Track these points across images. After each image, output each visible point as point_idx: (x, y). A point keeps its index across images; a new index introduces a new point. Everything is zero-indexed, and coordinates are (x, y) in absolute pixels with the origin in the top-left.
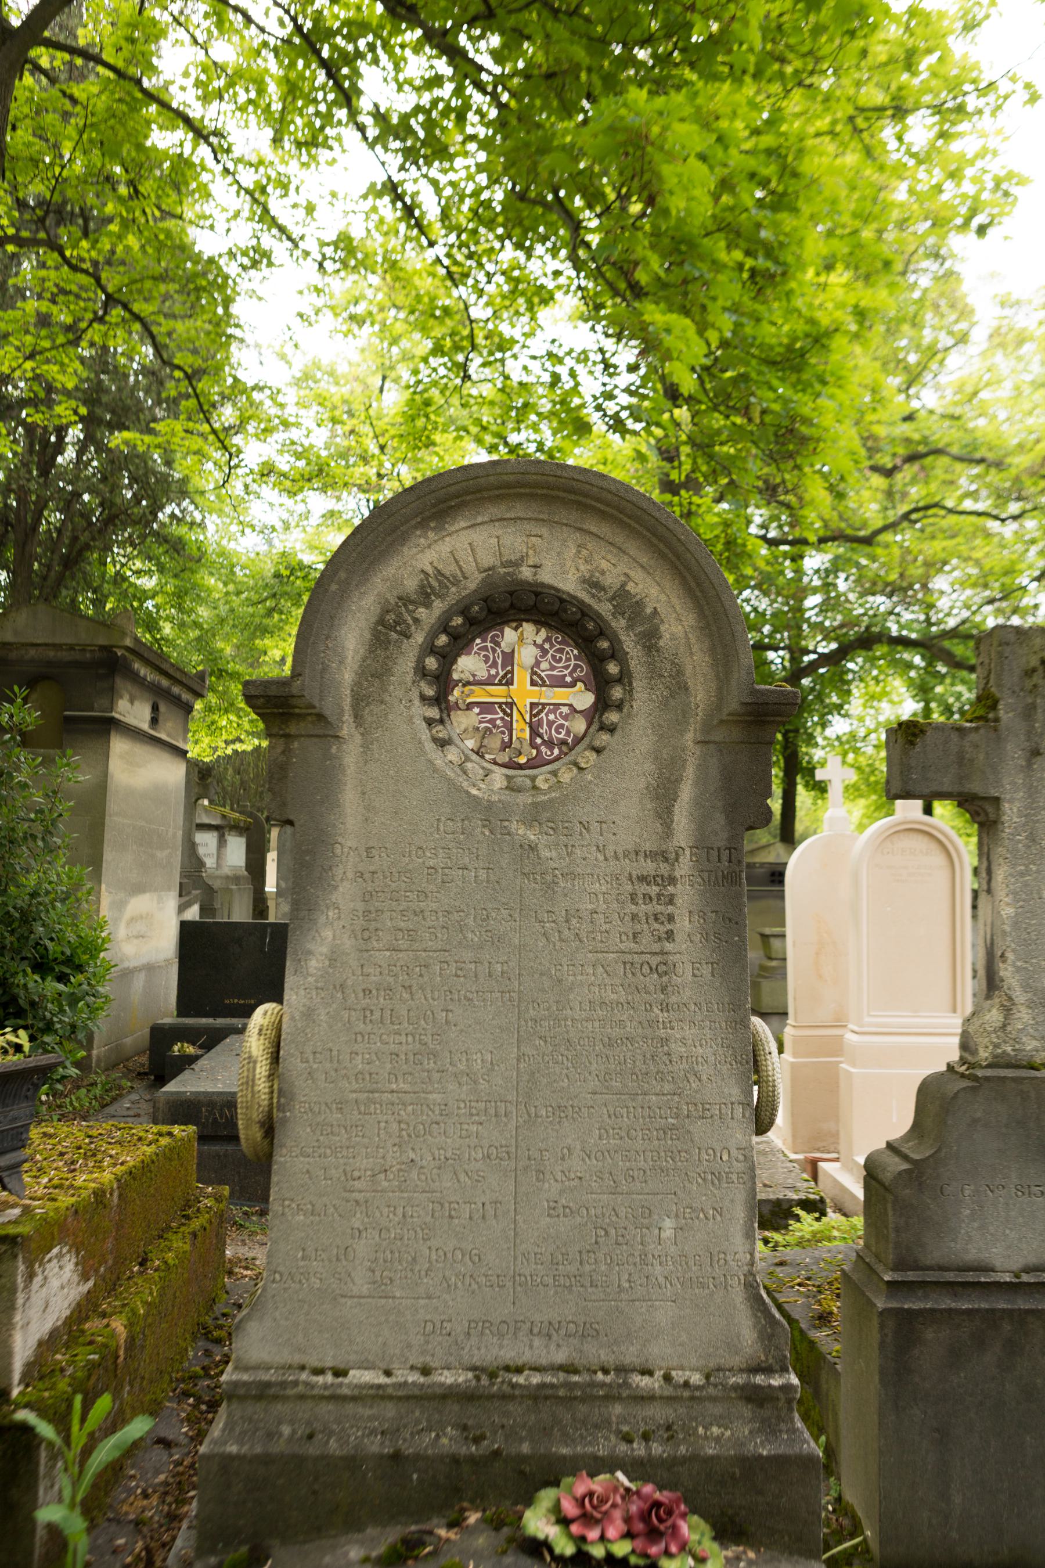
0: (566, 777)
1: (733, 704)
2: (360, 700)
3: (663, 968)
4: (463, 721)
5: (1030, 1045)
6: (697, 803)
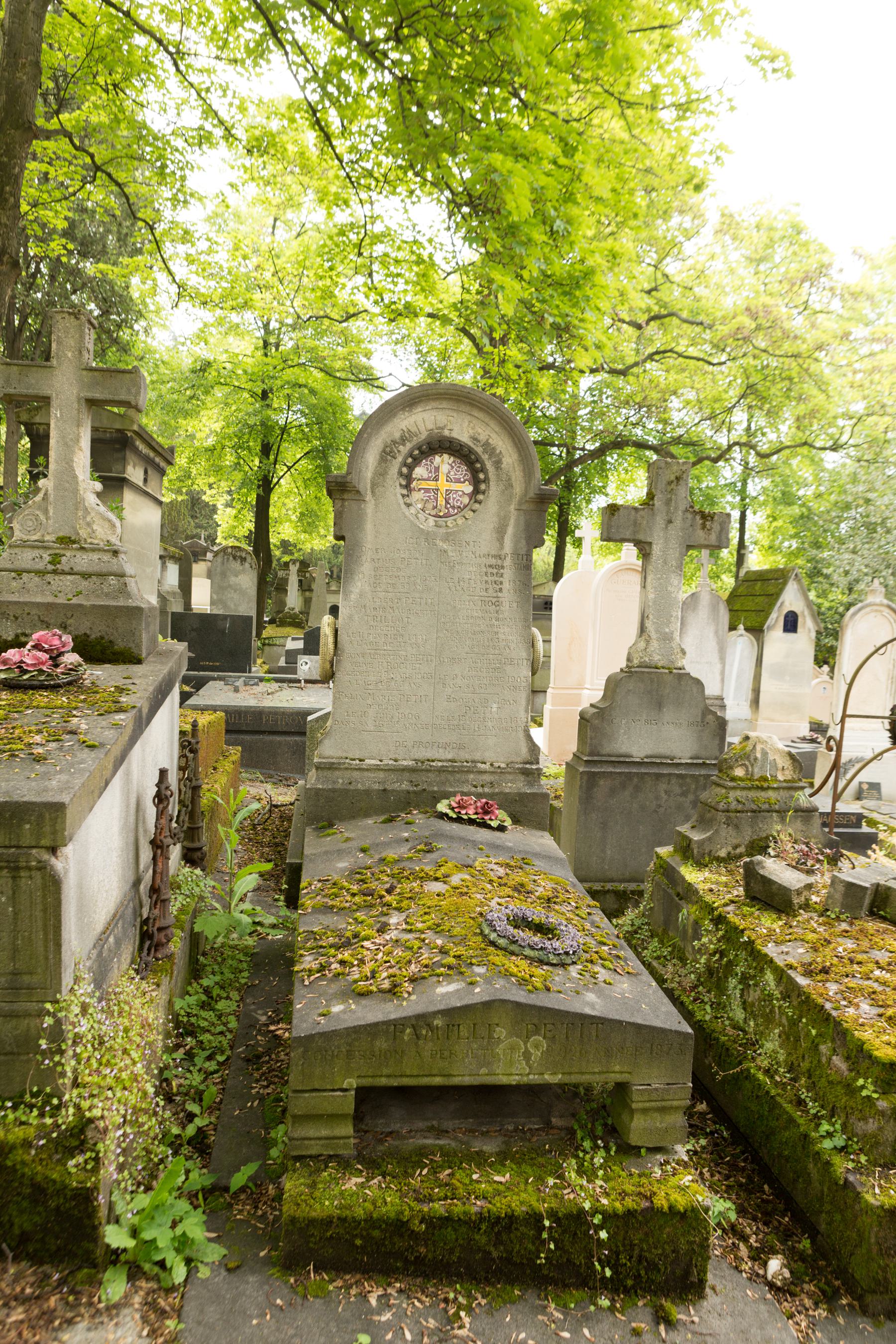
0: (460, 522)
1: (531, 494)
2: (374, 485)
3: (497, 604)
4: (416, 496)
5: (656, 658)
6: (515, 535)
